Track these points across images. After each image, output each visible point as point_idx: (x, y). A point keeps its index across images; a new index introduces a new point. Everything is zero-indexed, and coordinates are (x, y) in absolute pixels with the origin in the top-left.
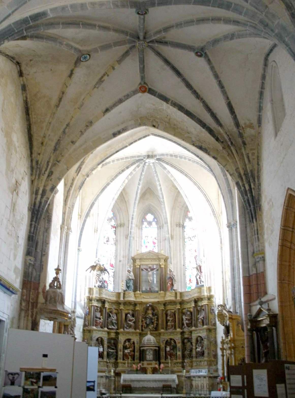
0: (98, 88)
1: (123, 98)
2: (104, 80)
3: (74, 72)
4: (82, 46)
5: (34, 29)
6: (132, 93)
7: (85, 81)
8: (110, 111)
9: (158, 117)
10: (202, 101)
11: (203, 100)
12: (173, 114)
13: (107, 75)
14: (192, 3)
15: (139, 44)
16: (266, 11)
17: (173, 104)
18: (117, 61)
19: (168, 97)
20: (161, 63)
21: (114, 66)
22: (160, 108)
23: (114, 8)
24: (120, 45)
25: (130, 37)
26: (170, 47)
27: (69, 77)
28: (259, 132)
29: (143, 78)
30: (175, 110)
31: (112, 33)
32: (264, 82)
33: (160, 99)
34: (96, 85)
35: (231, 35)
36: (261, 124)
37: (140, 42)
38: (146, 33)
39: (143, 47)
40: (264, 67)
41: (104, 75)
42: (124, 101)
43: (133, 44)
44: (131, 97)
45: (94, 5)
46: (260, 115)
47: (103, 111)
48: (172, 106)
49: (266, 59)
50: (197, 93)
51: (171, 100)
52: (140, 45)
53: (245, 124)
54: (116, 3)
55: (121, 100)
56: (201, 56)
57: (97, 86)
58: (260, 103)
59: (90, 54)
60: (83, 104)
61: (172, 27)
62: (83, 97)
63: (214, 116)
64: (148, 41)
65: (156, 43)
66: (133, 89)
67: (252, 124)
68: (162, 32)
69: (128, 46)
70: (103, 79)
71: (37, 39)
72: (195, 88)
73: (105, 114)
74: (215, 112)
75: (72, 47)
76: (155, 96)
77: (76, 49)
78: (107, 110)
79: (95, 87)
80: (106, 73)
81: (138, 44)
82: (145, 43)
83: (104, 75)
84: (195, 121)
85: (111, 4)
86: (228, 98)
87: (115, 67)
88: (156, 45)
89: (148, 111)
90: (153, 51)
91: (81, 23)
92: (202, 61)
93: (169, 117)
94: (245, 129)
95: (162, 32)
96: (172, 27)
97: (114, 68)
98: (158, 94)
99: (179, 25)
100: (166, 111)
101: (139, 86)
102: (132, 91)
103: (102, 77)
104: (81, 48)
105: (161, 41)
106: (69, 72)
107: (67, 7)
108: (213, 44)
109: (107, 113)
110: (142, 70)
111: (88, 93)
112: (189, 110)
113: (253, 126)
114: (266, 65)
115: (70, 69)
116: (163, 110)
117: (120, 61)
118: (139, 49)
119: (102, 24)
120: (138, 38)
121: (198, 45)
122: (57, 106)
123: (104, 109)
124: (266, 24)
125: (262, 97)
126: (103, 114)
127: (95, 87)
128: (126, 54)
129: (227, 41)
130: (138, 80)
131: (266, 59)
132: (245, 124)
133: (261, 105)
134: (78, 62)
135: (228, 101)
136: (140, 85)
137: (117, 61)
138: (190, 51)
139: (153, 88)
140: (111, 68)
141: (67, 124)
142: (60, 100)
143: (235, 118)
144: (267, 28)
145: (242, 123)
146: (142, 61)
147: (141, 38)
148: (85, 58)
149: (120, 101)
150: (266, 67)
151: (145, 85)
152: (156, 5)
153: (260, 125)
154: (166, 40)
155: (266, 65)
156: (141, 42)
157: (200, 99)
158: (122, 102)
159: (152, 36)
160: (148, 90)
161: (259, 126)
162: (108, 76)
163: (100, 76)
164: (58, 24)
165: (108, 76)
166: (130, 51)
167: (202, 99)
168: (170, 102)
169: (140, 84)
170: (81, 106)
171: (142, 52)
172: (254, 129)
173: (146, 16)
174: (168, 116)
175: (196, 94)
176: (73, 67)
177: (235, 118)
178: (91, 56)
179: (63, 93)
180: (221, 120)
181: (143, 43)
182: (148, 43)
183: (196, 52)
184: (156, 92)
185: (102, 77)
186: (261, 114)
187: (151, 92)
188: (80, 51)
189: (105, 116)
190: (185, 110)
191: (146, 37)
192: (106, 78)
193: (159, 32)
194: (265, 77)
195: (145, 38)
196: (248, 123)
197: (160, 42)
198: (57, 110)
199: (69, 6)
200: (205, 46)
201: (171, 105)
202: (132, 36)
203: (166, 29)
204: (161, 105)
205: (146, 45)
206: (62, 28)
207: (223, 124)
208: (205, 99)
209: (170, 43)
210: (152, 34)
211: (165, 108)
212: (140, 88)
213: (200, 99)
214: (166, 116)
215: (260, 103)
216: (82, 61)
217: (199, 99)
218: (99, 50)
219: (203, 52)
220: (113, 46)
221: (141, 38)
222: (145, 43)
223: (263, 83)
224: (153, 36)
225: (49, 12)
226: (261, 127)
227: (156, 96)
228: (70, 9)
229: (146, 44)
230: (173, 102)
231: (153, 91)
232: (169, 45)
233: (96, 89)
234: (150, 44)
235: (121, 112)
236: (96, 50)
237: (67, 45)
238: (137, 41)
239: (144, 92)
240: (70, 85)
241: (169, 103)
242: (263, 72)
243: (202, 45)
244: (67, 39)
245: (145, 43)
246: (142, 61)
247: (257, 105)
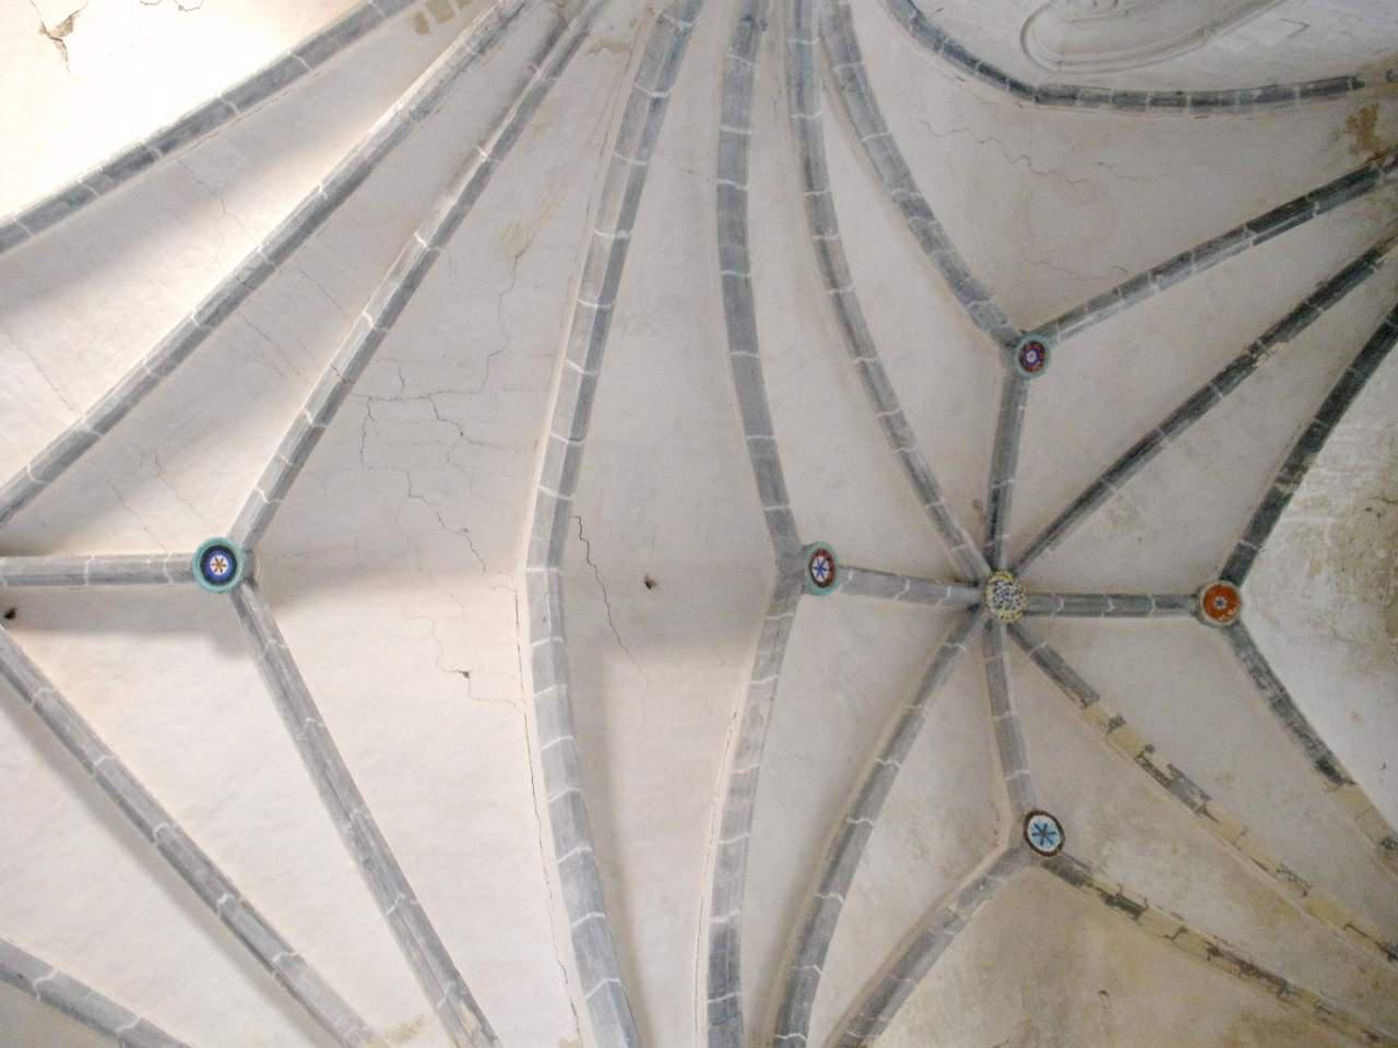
0: (1205, 797)
1: (1269, 693)
2: (1170, 766)
3: (1113, 890)
4: (995, 845)
5: (798, 997)
6: (1243, 655)
7: (1175, 851)
8: (1330, 753)
9: (1382, 554)
10: (1264, 347)
11: (1260, 343)
12: (1357, 482)
13: (1147, 755)
14: (751, 355)
15: (999, 607)
16: (672, 20)
17: (1293, 474)
18: (1086, 705)
19: (1259, 500)
20: (1096, 519)
21: (1107, 722)
22: (1328, 541)
23: (778, 672)
24: (1004, 683)
25: (961, 641)
26: (1011, 481)
27: (1141, 918)
28: (1384, 80)
29: (1169, 604)
30: (1320, 466)
31: (930, 713)
32: (1148, 100)
33: (1268, 531)
34: (1192, 805)
35: (912, 215)
36: (1345, 78)
37: (991, 604)
38: (957, 580)
39: (1017, 592)
40: (1078, 103)
41: (1148, 766)
42: (1282, 689)
43: (1003, 630)
44: (1261, 658)
45: (748, 748)
46: (1305, 94)
47: (1332, 785)
48: (1300, 476)
49: (1044, 96)
50: (1229, 369)
51: (1278, 485)
52: (1005, 604)
53: (1354, 151)
54: (762, 663)
55: (1280, 701)
56: (1041, 351)
57: (1199, 801)
58: (1247, 101)
59: (1028, 810)
60: (1282, 870)
61: (907, 461)
62: (1252, 870)
63: (1328, 292)
64: (986, 570)
65: (997, 537)
66: (1223, 644)
67: (1351, 122)
68: (936, 504)
69: (1009, 653)
70: (1167, 773)
71: (888, 1010)
72: (1206, 378)
73: (1343, 776)
74: (1312, 290)
75: (984, 882)
76: (1253, 553)
77: (997, 869)
78: (1326, 767)
79: (1203, 811)
80: (1140, 756)
81: (1001, 613)
82: (994, 579)
83: (1148, 766)
84: (1367, 375)
85: (763, 682)
86: (1234, 234)
87: (1112, 715)
88: (1006, 536)
89: (1353, 598)
90: (1039, 554)
91: (850, 820)
92: (1058, 351)
93: (1379, 506)
94: (1382, 149)
95: (936, 504)
96: (907, 461)
97: (1117, 723)
98: (1246, 539)
99: (895, 430)
100: (1342, 515)
101: (1208, 618)
102: (1237, 654)
103: (1158, 774)
104: (1003, 847)
105: (991, 517)
106: (1118, 914)
107: (725, 849)
108: (975, 297)
109: (1336, 768)
110: (1131, 604)
111: (1234, 844)
112: (1316, 409)
113: (1364, 111)
114: (1069, 96)
115: (1101, 904)
116: (1342, 528)
117: (1085, 696)
118: (1025, 613)
119: (882, 743)
120: (974, 608)
121: (996, 368)
122: (1280, 987)
123: (1319, 780)
124: (747, 25)
125: (1221, 97)
126: (1345, 787)
127: (1203, 811)
128: (1049, 663)
129: (940, 230)
130: (1182, 621)
131: (1044, 96)
132: (1354, 151)
133: (1258, 93)
134: (1060, 865)
135: (1246, 229)
136: (1203, 612)
137: (1086, 705)
138: (1023, 393)
139: (1222, 566)
140: (1117, 731)
141: (1386, 955)
142: (1248, 969)
143: (1325, 195)
144: (758, 19)
145: (1350, 165)
146: (1089, 604)
147: (971, 595)
148: (1043, 833)
149: (1282, 704)
150: (1079, 95)
151: (1203, 594)
152: (781, 507)
153: (1349, 82)
154: (985, 499)
155: (1069, 96)
156: (990, 596)
157: (1254, 356)
158: (1287, 697)
159: (961, 552)
160: (1227, 584)
161: (1357, 85)
162: (1150, 749)
163: (1157, 790)
164: (819, 904)
165: (1150, 749)
166: (1036, 648)
167: (1255, 349)
168: (1282, 488)
169: (1196, 614)
170: (1293, 879)
171: (1041, 602)
172: (1376, 107)
173: (841, 559)
174: (1369, 510)
175: (1232, 373)
176: (1095, 893)
177: (1325, 195)
178: (1041, 807)
179: (1214, 951)
180: (1349, 262)
181: (995, 590)
182: (994, 569)
183: (1021, 371)
184: (1240, 547)
185: (1158, 774)
186: (1297, 89)
187: (1237, 568)
188: (1011, 854)
189: (1355, 777)
190: (1318, 421)
191: (971, 578)
192: (1159, 760)
193: (940, 518)
194: (1125, 95)
195: (975, 584)
196: (1349, 140)
197: (994, 521)
198: (1300, 993)
199: (722, 842)
200: (994, 334)
201: (1298, 483)
202: (962, 631)
203: (926, 489)
204: (1313, 537)
205: (1006, 581)
206: (844, 893)
207: (1366, 248)
208: (1251, 337)
209: (998, 483)
210: (954, 549)
211: (1330, 520)
212: (1215, 614)
213: (1254, 356)
214: (1373, 516)
215: (1247, 101)
216: (1060, 846)
217: (1255, 361)
218: (1017, 772)
219: (1018, 340)
220: (1007, 714)
221: (971, 595)
222: (996, 583)
223: (1158, 101)
224: (962, 547)
225: (721, 920)
226: (1359, 74)
227: (1255, 548)
228: (735, 840)
229: (1003, 578)
230: (1281, 474)
231: (1233, 560)
232: (1004, 483)
233: (1212, 807)
234: (1003, 562)
235: (1355, 717)
236: (1017, 788)
237: (966, 899)
238: (984, 616)
239: (1233, 600)
240: (1181, 918)
241: (1288, 492)
242: (1103, 106)
243: (996, 348)
244: (943, 898)
245: (994, 579)
246: (1089, 604)
247: (1259, 111)
